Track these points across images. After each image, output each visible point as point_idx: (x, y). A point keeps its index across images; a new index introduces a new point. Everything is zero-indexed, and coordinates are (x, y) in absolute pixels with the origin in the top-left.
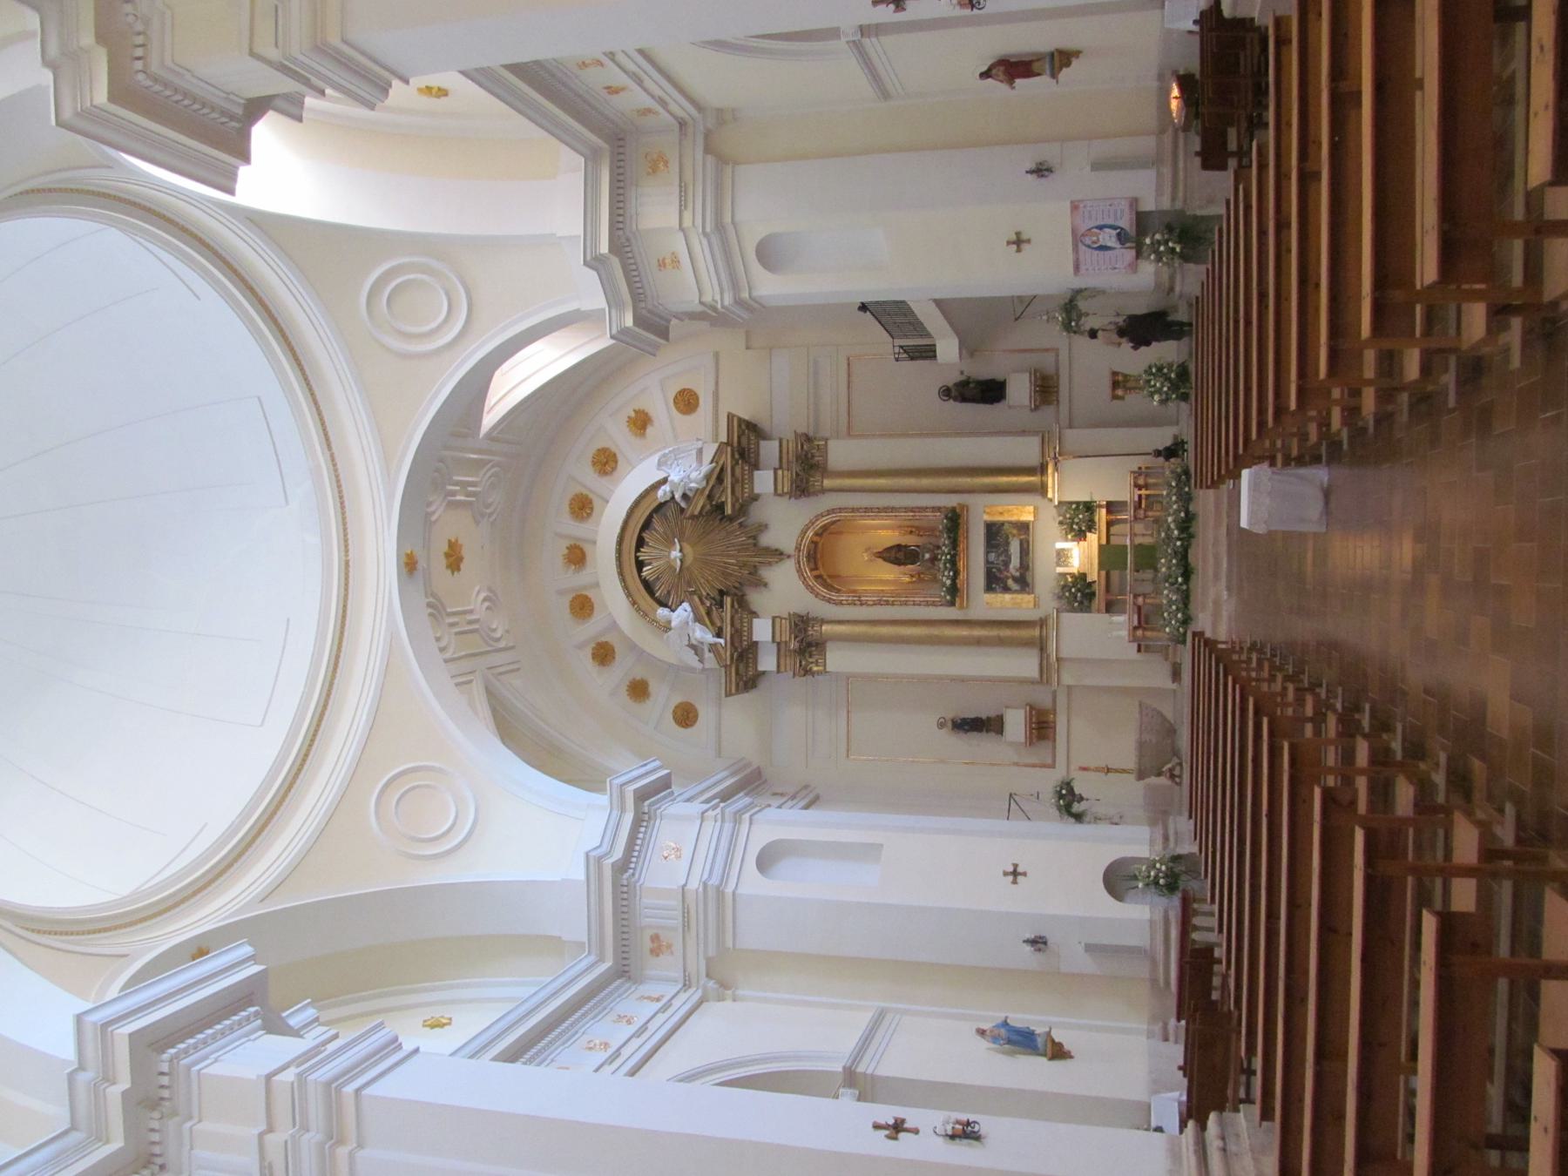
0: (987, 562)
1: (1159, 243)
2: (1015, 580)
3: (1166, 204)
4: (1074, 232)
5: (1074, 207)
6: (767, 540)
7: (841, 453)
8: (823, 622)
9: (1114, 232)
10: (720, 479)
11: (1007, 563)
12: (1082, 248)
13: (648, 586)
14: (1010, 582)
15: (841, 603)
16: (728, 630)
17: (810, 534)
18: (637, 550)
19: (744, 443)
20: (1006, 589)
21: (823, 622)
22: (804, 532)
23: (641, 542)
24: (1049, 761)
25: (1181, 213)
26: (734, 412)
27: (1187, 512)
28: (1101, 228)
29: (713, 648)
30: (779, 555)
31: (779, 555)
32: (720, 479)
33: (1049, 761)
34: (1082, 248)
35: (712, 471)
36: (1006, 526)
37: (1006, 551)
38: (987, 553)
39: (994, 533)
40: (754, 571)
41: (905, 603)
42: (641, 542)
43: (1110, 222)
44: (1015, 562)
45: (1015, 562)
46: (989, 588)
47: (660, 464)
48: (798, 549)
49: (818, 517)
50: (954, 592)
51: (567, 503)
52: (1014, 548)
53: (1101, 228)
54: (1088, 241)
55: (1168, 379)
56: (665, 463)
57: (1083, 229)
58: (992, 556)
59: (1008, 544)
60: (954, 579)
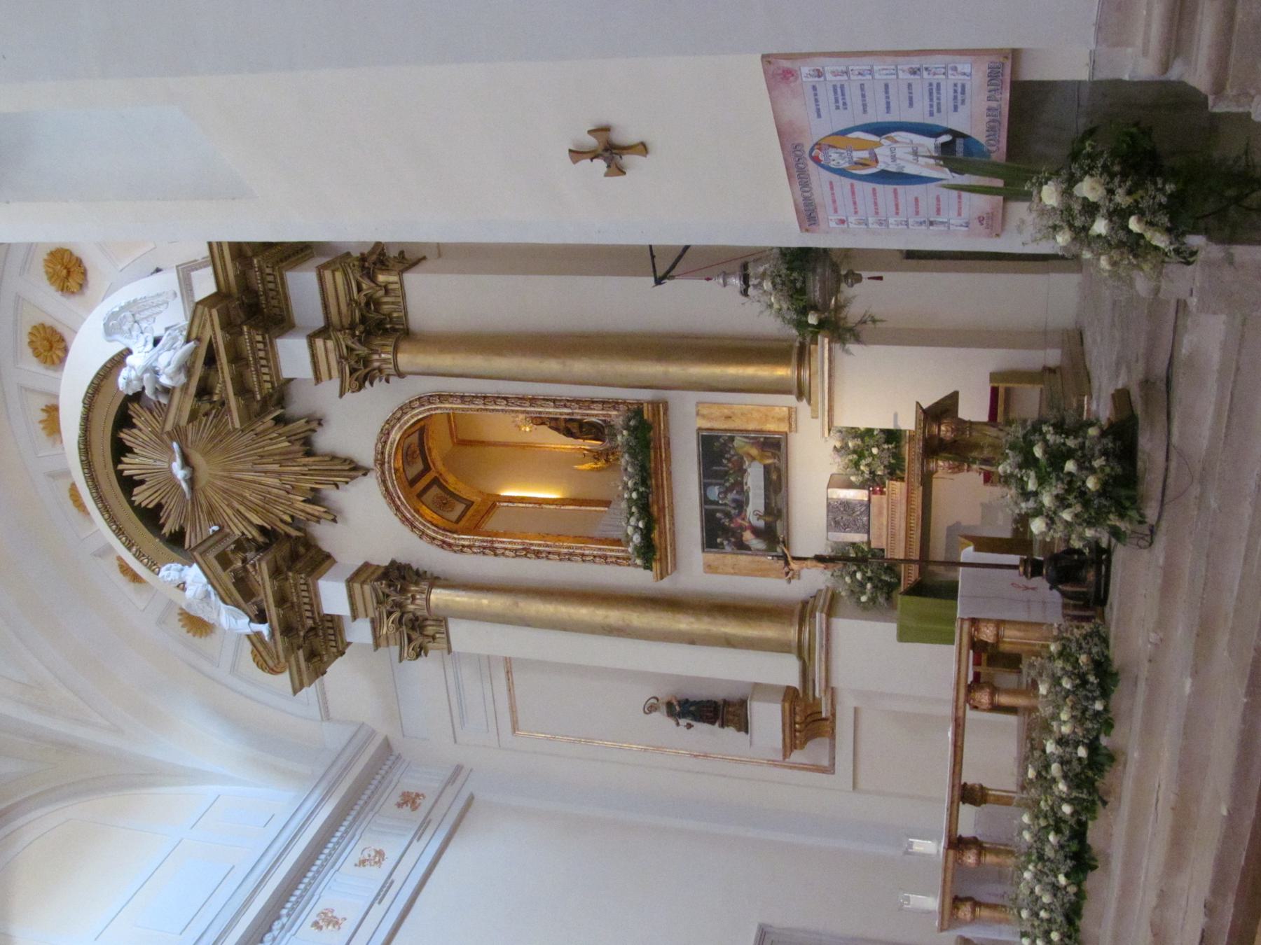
0: (705, 500)
1: (1091, 209)
2: (757, 532)
3: (1137, 63)
4: (785, 134)
5: (779, 71)
6: (326, 440)
7: (427, 298)
8: (436, 581)
9: (929, 143)
10: (211, 360)
11: (741, 505)
12: (820, 178)
13: (151, 517)
14: (748, 536)
15: (462, 549)
16: (273, 612)
17: (396, 435)
18: (117, 460)
19: (249, 291)
20: (742, 546)
21: (436, 581)
22: (385, 433)
23: (120, 450)
24: (825, 762)
25: (1176, 100)
26: (215, 239)
27: (1093, 747)
28: (881, 130)
29: (255, 639)
30: (354, 469)
31: (354, 469)
32: (211, 360)
33: (825, 762)
34: (820, 178)
35: (194, 353)
36: (739, 442)
37: (739, 486)
38: (704, 487)
39: (716, 454)
40: (315, 498)
41: (570, 557)
42: (120, 450)
43: (917, 115)
44: (756, 503)
45: (756, 503)
46: (710, 542)
47: (110, 331)
48: (381, 461)
49: (404, 409)
50: (650, 551)
51: (26, 339)
52: (754, 479)
53: (881, 130)
54: (835, 158)
55: (1073, 488)
56: (119, 329)
57: (819, 129)
58: (714, 492)
59: (742, 472)
60: (646, 534)
